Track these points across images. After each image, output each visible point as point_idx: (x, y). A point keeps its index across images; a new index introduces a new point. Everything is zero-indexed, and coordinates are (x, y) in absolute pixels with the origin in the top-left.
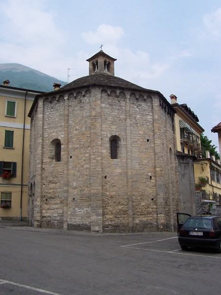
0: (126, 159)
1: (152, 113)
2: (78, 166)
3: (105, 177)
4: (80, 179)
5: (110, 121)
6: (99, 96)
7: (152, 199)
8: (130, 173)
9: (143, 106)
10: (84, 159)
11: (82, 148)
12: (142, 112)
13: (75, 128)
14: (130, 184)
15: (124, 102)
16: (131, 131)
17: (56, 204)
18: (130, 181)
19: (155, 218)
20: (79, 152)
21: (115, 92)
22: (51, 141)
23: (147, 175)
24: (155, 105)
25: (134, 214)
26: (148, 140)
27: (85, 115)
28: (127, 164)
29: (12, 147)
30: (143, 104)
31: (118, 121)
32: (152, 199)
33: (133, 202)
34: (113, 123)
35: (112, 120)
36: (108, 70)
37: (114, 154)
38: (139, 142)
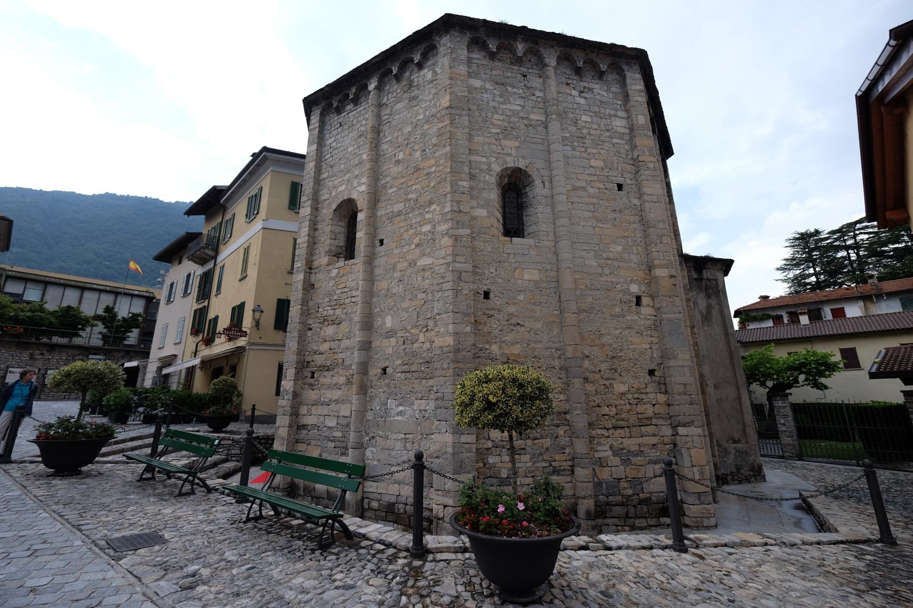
0: (551, 237)
1: (627, 111)
3: (487, 295)
4: (406, 305)
5: (499, 126)
6: (463, 53)
7: (651, 373)
8: (568, 282)
9: (595, 91)
10: (416, 241)
11: (413, 210)
12: (596, 109)
13: (394, 160)
14: (571, 318)
15: (541, 80)
16: (566, 157)
17: (336, 386)
18: (573, 307)
19: (666, 440)
20: (402, 224)
21: (512, 50)
22: (334, 206)
23: (626, 292)
24: (634, 87)
25: (591, 425)
26: (620, 187)
28: (556, 253)
30: (599, 89)
31: (523, 126)
32: (651, 373)
33: (586, 379)
34: (506, 133)
35: (506, 124)
37: (514, 226)
38: (591, 190)
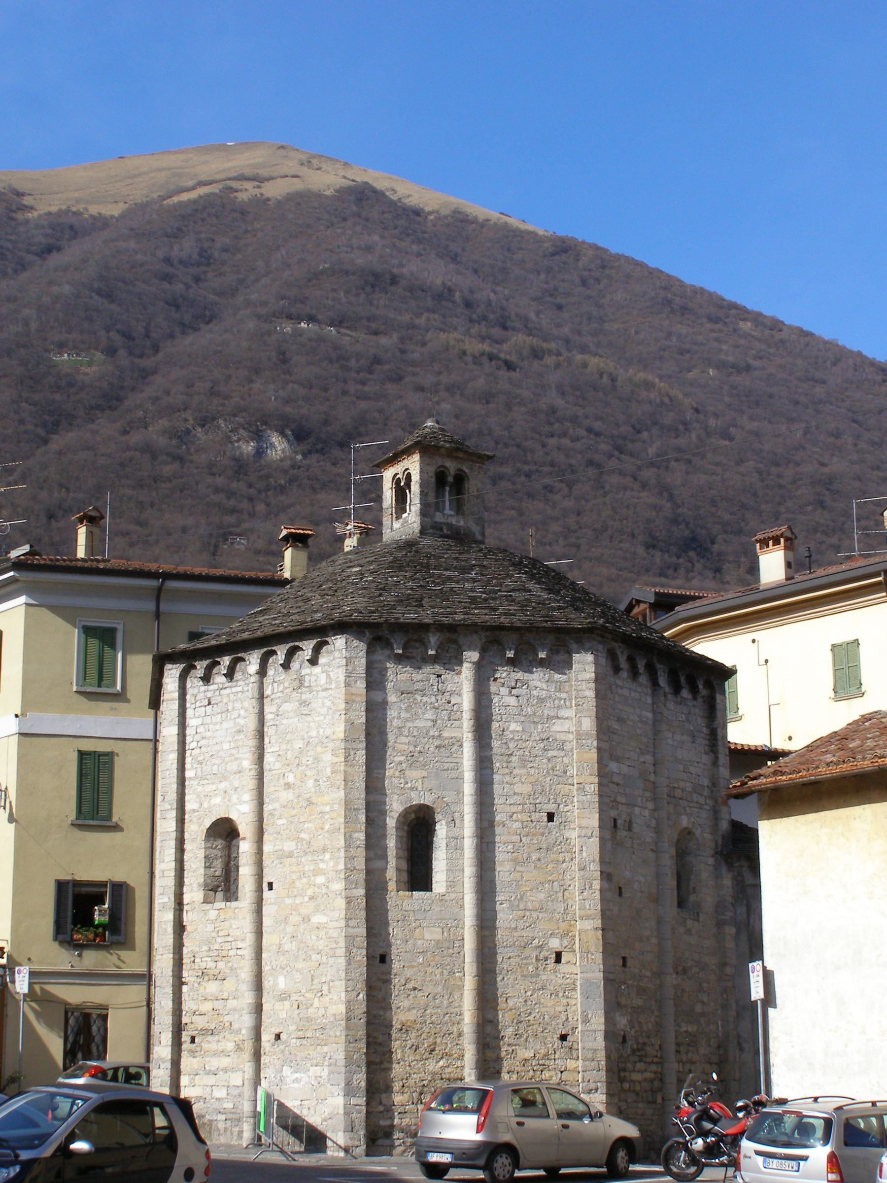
2: (295, 919)
4: (300, 965)
10: (310, 892)
17: (223, 1053)
20: (294, 868)
27: (314, 734)
29: (109, 817)
35: (411, 748)
36: (459, 508)
